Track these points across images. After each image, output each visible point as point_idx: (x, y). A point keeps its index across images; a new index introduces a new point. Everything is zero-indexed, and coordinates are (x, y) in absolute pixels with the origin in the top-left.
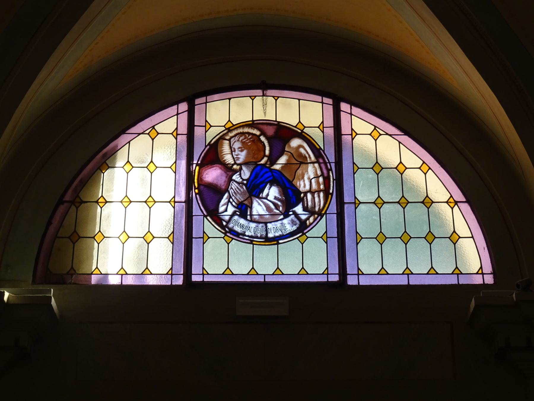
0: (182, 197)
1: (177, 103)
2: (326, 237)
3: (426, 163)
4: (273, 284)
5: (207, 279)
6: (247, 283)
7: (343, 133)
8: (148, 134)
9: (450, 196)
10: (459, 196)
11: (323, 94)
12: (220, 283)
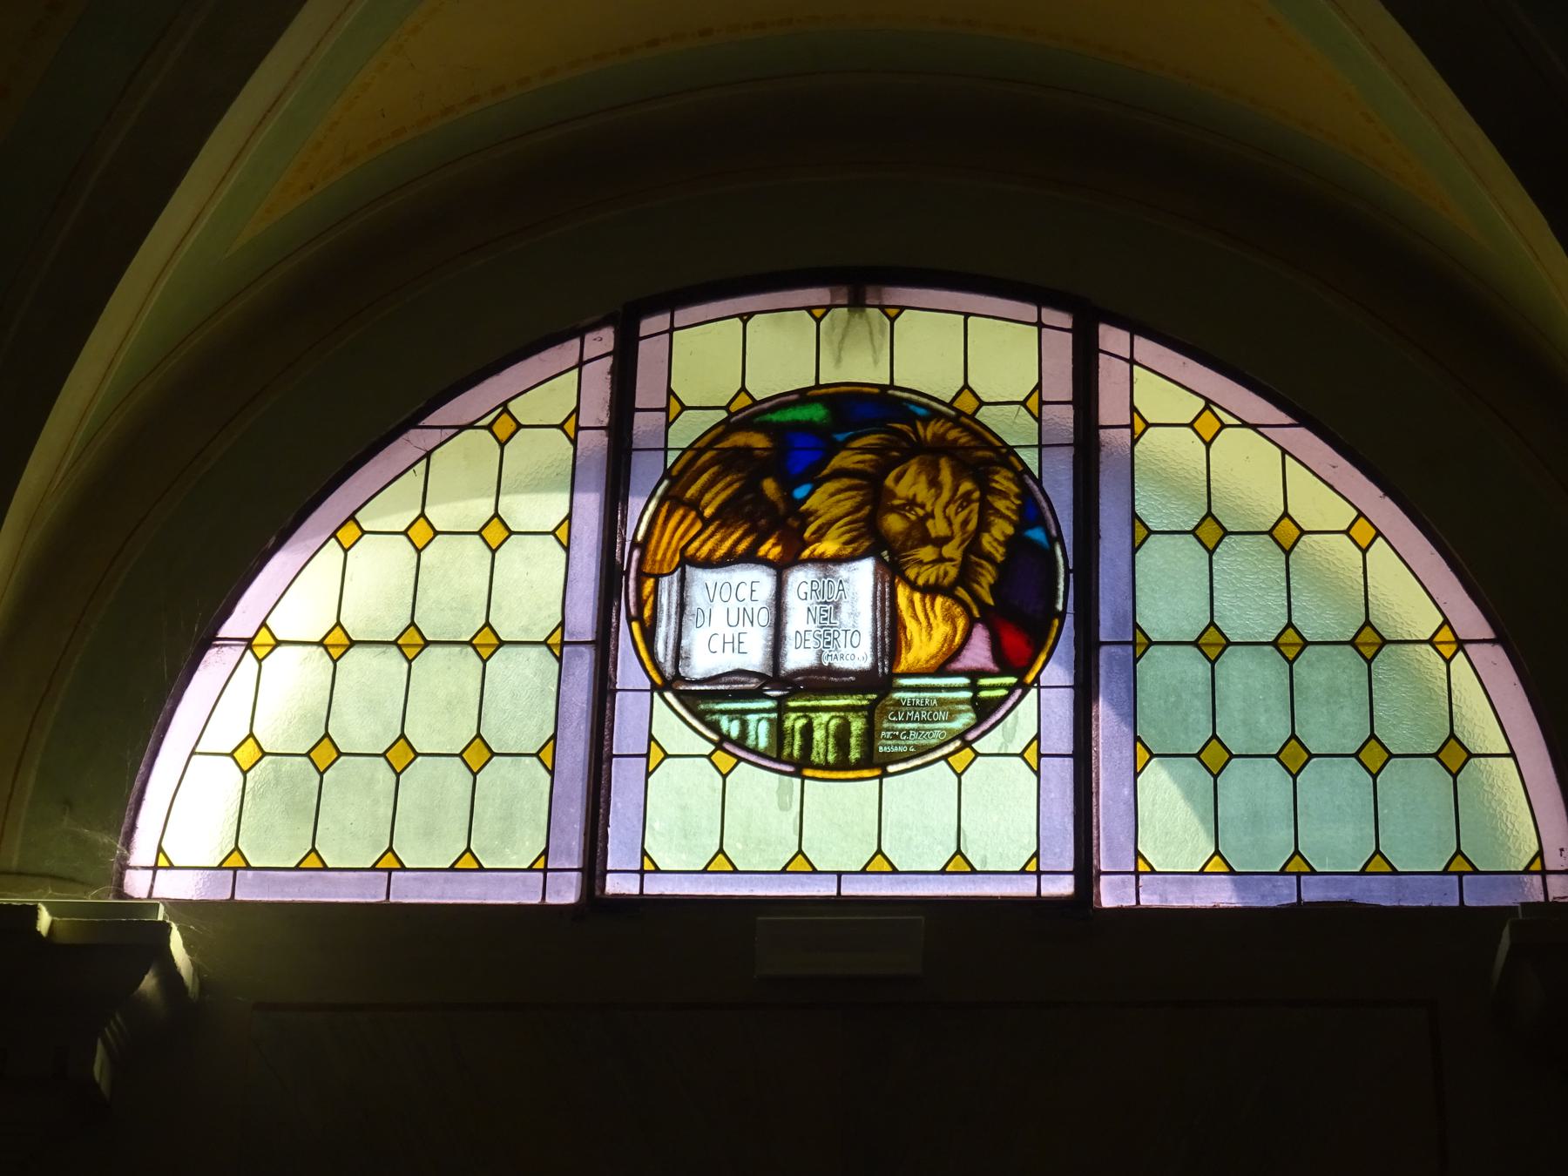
0: (584, 623)
1: (580, 333)
2: (1035, 755)
3: (431, 463)
4: (968, 901)
5: (655, 887)
6: (809, 900)
7: (1102, 422)
8: (489, 427)
9: (1440, 619)
10: (1472, 621)
11: (1041, 296)
12: (974, 901)
